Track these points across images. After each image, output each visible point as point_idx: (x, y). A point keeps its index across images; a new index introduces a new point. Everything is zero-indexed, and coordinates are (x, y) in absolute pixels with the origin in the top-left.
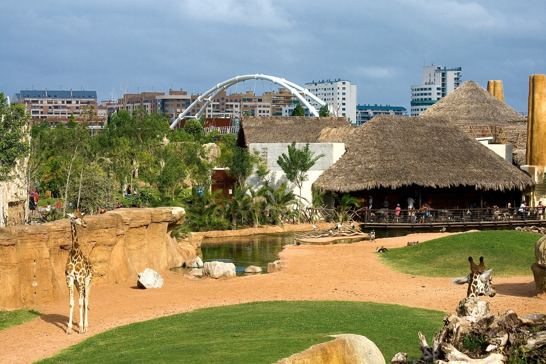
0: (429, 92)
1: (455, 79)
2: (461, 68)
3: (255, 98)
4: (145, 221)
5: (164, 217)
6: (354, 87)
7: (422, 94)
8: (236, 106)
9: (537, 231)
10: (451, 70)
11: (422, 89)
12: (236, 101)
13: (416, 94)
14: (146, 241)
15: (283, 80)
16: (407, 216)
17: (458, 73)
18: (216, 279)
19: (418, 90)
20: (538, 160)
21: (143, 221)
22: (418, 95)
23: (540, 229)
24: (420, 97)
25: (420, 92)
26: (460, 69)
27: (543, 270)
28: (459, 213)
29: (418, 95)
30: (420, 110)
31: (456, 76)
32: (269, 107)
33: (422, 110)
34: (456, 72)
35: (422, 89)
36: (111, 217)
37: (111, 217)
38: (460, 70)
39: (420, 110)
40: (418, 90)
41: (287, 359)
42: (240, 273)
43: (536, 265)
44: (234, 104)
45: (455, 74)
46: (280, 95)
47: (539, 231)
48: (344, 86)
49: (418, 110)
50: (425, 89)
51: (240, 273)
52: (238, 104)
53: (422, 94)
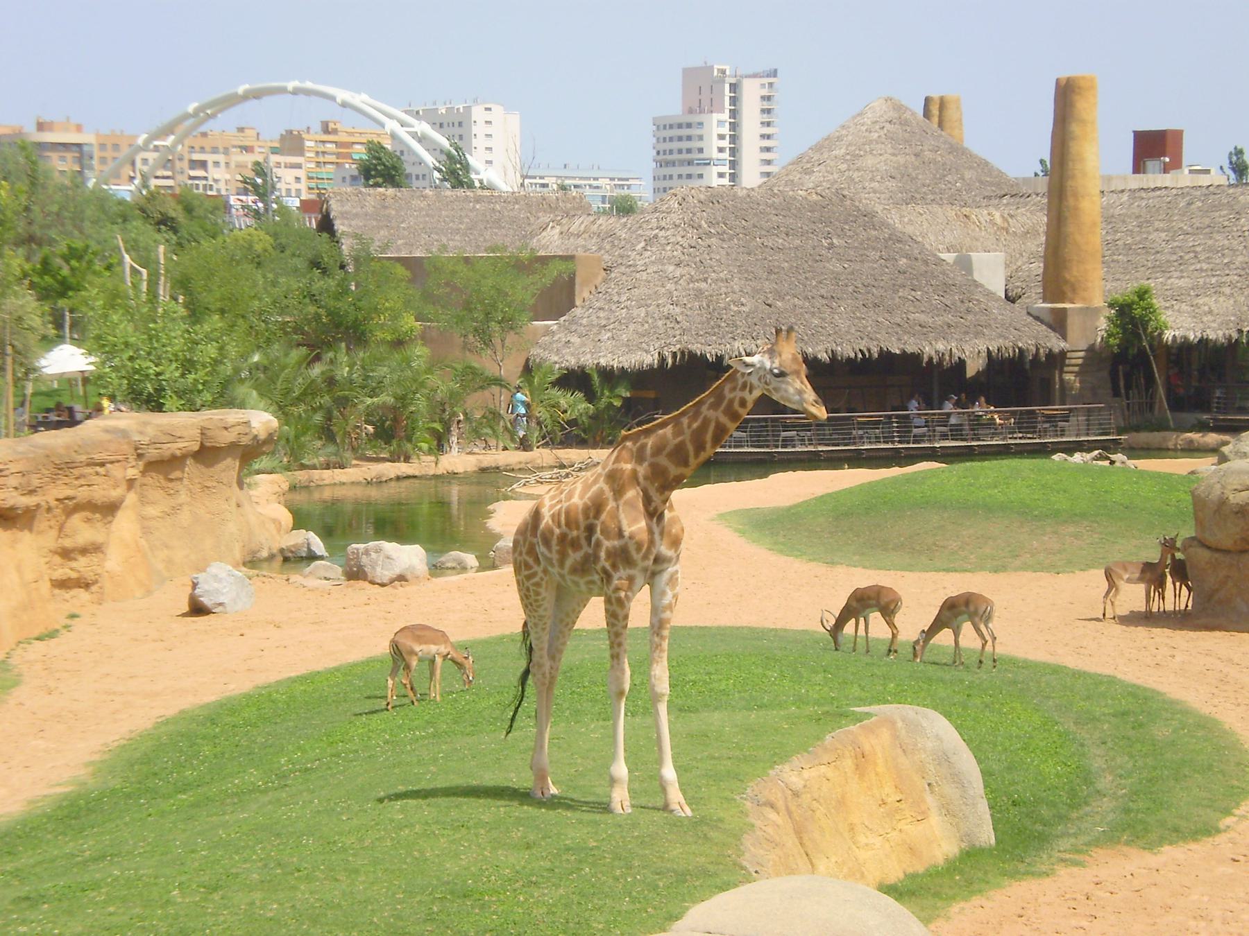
0: (698, 132)
1: (763, 98)
2: (776, 71)
3: (260, 144)
4: (186, 444)
5: (229, 437)
6: (514, 121)
7: (680, 139)
8: (216, 164)
9: (1106, 463)
10: (755, 76)
11: (680, 126)
12: (215, 150)
13: (665, 139)
14: (183, 497)
15: (364, 97)
16: (1036, 422)
17: (771, 84)
18: (383, 585)
19: (671, 127)
20: (1074, 290)
21: (181, 445)
22: (671, 139)
23: (1113, 457)
24: (676, 145)
25: (676, 132)
26: (774, 73)
27: (1217, 555)
28: (746, 427)
29: (671, 139)
30: (675, 177)
31: (765, 92)
32: (301, 168)
33: (680, 176)
34: (766, 81)
35: (680, 126)
36: (108, 437)
37: (108, 437)
38: (775, 76)
39: (675, 177)
40: (671, 127)
41: (787, 767)
42: (436, 569)
43: (1196, 542)
44: (210, 158)
45: (763, 85)
46: (325, 137)
47: (1112, 462)
48: (488, 117)
49: (671, 177)
50: (689, 125)
51: (436, 569)
52: (221, 158)
53: (680, 139)
